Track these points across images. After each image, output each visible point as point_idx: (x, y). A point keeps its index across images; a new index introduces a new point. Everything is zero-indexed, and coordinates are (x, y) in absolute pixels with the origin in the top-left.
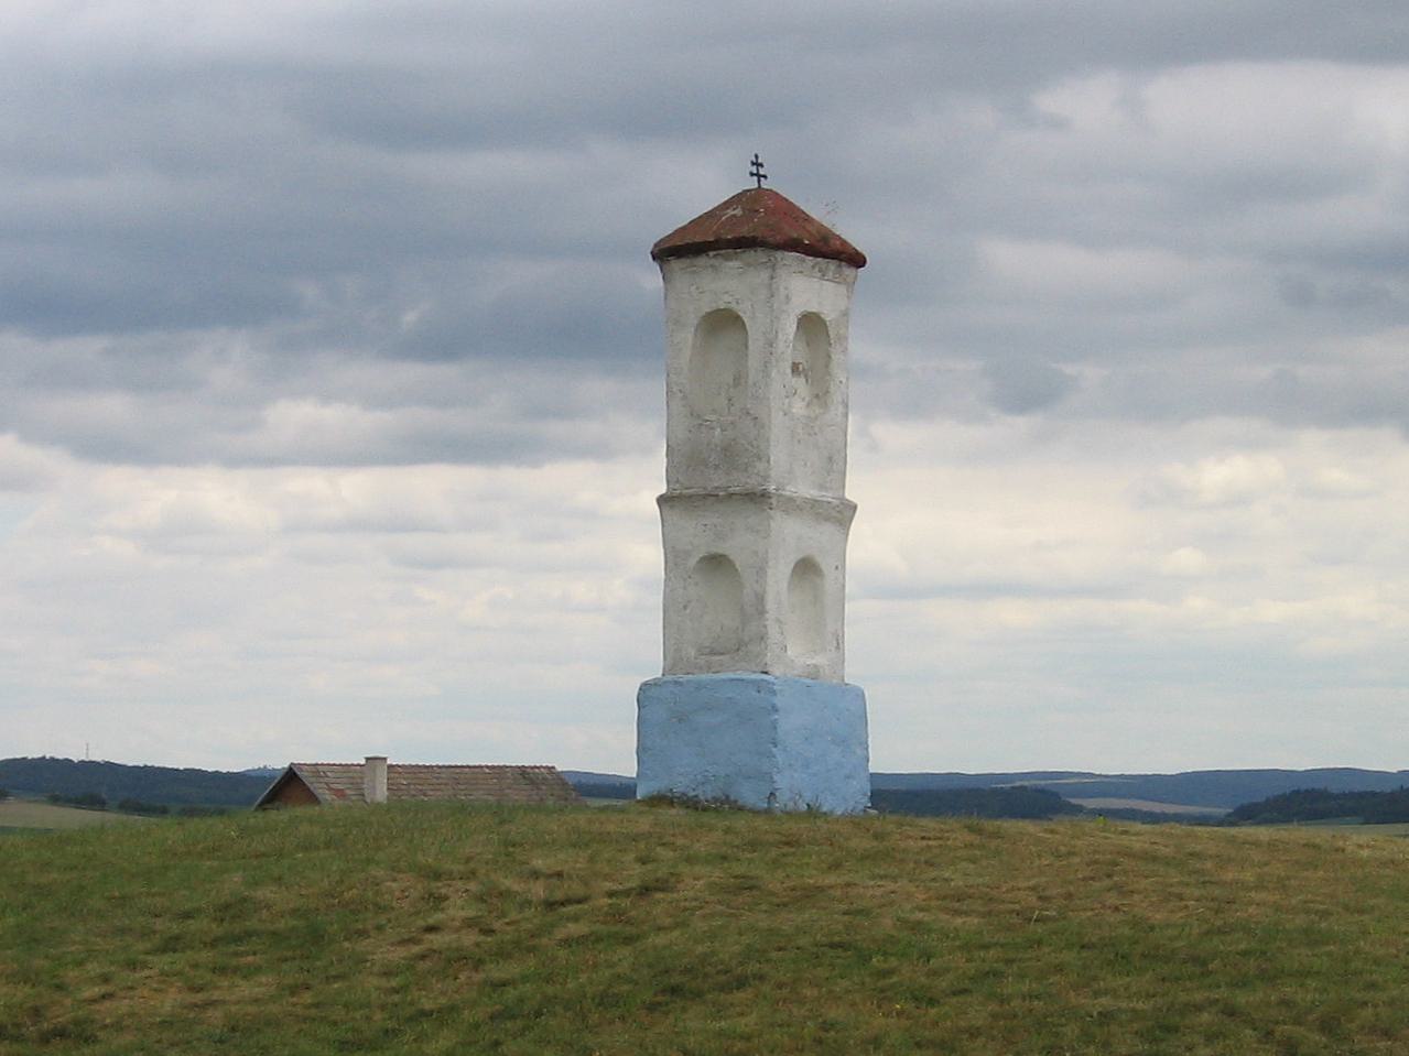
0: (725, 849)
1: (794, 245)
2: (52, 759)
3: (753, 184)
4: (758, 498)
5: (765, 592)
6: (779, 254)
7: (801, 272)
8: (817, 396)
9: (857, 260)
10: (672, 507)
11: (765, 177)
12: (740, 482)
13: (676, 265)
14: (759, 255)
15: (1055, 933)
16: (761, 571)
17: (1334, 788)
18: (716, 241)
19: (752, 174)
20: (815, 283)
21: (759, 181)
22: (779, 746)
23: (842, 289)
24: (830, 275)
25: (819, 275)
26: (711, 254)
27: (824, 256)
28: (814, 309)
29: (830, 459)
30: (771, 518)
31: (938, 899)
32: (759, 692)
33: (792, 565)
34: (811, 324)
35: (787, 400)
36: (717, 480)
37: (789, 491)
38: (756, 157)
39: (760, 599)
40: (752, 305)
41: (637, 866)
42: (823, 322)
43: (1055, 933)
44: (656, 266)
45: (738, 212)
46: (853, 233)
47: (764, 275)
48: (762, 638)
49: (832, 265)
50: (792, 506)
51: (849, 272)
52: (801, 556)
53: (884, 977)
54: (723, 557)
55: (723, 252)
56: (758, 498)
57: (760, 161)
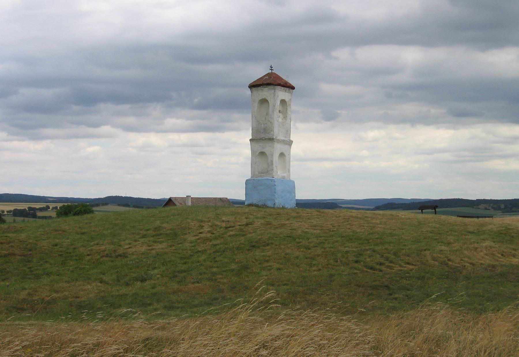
1: (279, 85)
3: (270, 71)
4: (271, 140)
6: (276, 87)
9: (293, 88)
11: (273, 70)
12: (267, 136)
13: (254, 89)
19: (270, 69)
20: (284, 93)
21: (272, 71)
23: (290, 94)
27: (286, 87)
34: (283, 102)
35: (278, 119)
36: (262, 136)
37: (278, 138)
38: (271, 65)
49: (288, 89)
50: (279, 141)
51: (291, 90)
55: (264, 86)
56: (271, 140)
57: (272, 66)
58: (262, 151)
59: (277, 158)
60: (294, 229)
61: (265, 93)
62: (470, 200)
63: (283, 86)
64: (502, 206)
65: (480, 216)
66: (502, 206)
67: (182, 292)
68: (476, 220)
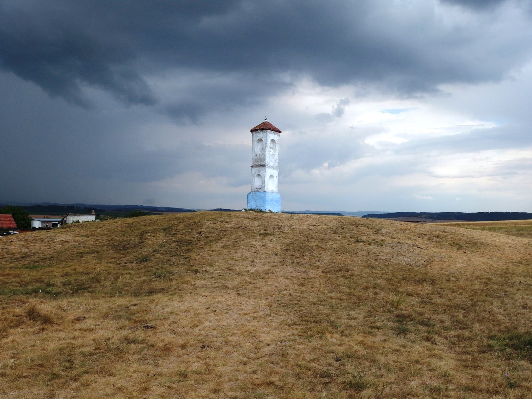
1: (269, 129)
2: (499, 212)
4: (264, 166)
6: (268, 131)
9: (280, 132)
12: (262, 163)
13: (254, 132)
14: (264, 131)
15: (257, 379)
17: (375, 214)
20: (274, 135)
23: (278, 136)
27: (275, 131)
34: (273, 141)
36: (259, 163)
39: (264, 180)
43: (257, 379)
44: (251, 133)
45: (263, 125)
46: (280, 130)
49: (276, 132)
50: (270, 167)
51: (279, 133)
56: (264, 166)
58: (258, 174)
59: (268, 179)
60: (500, 229)
61: (260, 135)
62: (503, 213)
63: (273, 130)
64: (435, 216)
65: (316, 215)
66: (435, 216)
67: (355, 276)
68: (335, 216)
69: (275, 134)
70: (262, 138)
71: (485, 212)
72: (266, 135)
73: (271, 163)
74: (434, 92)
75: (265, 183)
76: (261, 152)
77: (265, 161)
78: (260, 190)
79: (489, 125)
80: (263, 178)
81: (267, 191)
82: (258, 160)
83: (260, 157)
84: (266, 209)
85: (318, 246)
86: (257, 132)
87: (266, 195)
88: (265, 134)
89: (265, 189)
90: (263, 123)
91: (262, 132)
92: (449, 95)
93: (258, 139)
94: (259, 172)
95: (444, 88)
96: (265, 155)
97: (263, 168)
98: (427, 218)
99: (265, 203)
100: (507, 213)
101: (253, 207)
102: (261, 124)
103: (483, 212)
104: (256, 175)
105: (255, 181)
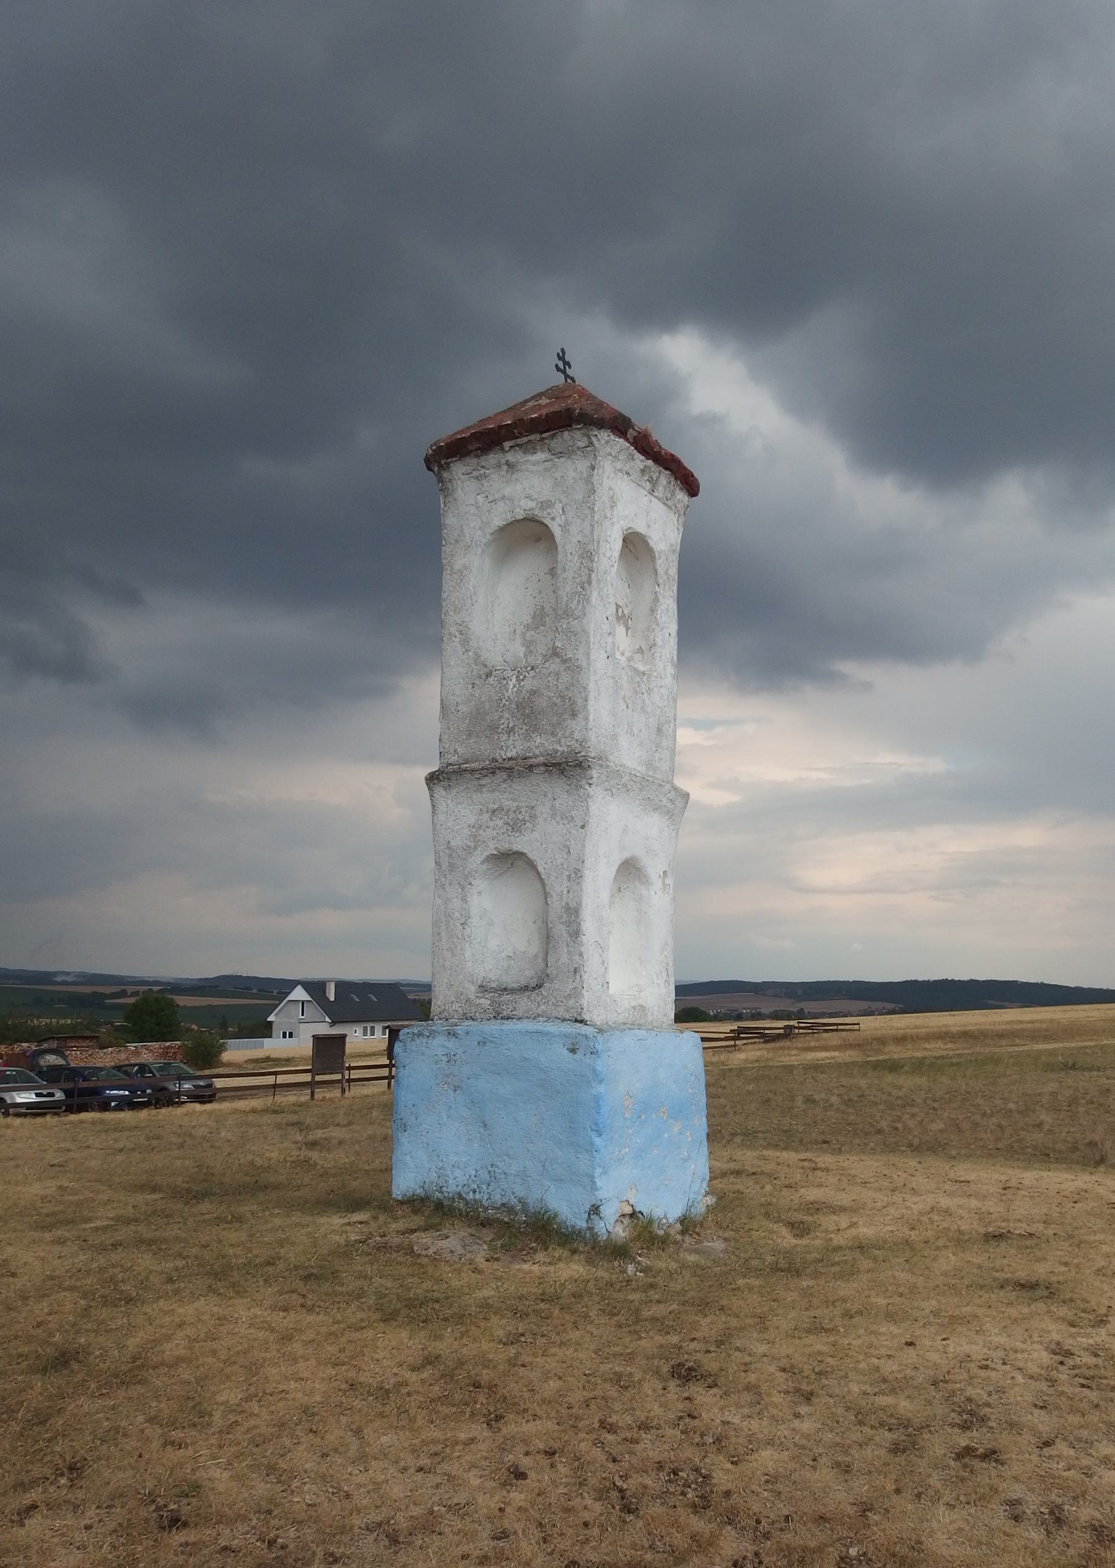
0: (896, 1341)
2: (953, 980)
5: (579, 904)
7: (628, 473)
8: (640, 650)
10: (447, 788)
12: (541, 745)
16: (577, 875)
18: (514, 425)
22: (604, 1136)
24: (660, 491)
25: (648, 485)
26: (507, 445)
28: (641, 528)
29: (659, 730)
30: (589, 796)
31: (165, 1241)
32: (573, 1051)
33: (615, 869)
36: (513, 747)
39: (573, 913)
40: (563, 509)
41: (803, 1413)
42: (650, 551)
47: (582, 465)
48: (576, 971)
49: (664, 478)
52: (626, 855)
53: (85, 1223)
54: (520, 855)
58: (505, 846)
59: (605, 895)
64: (800, 992)
66: (800, 992)
69: (654, 483)
70: (546, 505)
71: (920, 979)
72: (589, 480)
73: (624, 741)
74: (829, 679)
75: (576, 933)
76: (528, 645)
77: (575, 726)
78: (523, 1003)
79: (936, 766)
80: (558, 887)
81: (596, 1016)
82: (507, 719)
83: (529, 684)
84: (595, 1210)
85: (1095, 1560)
86: (492, 458)
87: (600, 1066)
88: (572, 469)
89: (576, 993)
90: (554, 393)
91: (540, 456)
92: (867, 686)
93: (498, 522)
94: (516, 826)
95: (847, 667)
96: (573, 668)
97: (557, 789)
98: (780, 997)
99: (592, 1149)
100: (972, 981)
101: (462, 1180)
102: (526, 401)
103: (916, 981)
104: (476, 860)
105: (474, 921)
